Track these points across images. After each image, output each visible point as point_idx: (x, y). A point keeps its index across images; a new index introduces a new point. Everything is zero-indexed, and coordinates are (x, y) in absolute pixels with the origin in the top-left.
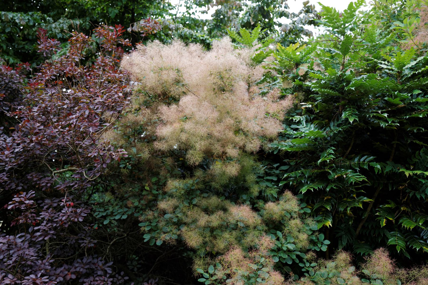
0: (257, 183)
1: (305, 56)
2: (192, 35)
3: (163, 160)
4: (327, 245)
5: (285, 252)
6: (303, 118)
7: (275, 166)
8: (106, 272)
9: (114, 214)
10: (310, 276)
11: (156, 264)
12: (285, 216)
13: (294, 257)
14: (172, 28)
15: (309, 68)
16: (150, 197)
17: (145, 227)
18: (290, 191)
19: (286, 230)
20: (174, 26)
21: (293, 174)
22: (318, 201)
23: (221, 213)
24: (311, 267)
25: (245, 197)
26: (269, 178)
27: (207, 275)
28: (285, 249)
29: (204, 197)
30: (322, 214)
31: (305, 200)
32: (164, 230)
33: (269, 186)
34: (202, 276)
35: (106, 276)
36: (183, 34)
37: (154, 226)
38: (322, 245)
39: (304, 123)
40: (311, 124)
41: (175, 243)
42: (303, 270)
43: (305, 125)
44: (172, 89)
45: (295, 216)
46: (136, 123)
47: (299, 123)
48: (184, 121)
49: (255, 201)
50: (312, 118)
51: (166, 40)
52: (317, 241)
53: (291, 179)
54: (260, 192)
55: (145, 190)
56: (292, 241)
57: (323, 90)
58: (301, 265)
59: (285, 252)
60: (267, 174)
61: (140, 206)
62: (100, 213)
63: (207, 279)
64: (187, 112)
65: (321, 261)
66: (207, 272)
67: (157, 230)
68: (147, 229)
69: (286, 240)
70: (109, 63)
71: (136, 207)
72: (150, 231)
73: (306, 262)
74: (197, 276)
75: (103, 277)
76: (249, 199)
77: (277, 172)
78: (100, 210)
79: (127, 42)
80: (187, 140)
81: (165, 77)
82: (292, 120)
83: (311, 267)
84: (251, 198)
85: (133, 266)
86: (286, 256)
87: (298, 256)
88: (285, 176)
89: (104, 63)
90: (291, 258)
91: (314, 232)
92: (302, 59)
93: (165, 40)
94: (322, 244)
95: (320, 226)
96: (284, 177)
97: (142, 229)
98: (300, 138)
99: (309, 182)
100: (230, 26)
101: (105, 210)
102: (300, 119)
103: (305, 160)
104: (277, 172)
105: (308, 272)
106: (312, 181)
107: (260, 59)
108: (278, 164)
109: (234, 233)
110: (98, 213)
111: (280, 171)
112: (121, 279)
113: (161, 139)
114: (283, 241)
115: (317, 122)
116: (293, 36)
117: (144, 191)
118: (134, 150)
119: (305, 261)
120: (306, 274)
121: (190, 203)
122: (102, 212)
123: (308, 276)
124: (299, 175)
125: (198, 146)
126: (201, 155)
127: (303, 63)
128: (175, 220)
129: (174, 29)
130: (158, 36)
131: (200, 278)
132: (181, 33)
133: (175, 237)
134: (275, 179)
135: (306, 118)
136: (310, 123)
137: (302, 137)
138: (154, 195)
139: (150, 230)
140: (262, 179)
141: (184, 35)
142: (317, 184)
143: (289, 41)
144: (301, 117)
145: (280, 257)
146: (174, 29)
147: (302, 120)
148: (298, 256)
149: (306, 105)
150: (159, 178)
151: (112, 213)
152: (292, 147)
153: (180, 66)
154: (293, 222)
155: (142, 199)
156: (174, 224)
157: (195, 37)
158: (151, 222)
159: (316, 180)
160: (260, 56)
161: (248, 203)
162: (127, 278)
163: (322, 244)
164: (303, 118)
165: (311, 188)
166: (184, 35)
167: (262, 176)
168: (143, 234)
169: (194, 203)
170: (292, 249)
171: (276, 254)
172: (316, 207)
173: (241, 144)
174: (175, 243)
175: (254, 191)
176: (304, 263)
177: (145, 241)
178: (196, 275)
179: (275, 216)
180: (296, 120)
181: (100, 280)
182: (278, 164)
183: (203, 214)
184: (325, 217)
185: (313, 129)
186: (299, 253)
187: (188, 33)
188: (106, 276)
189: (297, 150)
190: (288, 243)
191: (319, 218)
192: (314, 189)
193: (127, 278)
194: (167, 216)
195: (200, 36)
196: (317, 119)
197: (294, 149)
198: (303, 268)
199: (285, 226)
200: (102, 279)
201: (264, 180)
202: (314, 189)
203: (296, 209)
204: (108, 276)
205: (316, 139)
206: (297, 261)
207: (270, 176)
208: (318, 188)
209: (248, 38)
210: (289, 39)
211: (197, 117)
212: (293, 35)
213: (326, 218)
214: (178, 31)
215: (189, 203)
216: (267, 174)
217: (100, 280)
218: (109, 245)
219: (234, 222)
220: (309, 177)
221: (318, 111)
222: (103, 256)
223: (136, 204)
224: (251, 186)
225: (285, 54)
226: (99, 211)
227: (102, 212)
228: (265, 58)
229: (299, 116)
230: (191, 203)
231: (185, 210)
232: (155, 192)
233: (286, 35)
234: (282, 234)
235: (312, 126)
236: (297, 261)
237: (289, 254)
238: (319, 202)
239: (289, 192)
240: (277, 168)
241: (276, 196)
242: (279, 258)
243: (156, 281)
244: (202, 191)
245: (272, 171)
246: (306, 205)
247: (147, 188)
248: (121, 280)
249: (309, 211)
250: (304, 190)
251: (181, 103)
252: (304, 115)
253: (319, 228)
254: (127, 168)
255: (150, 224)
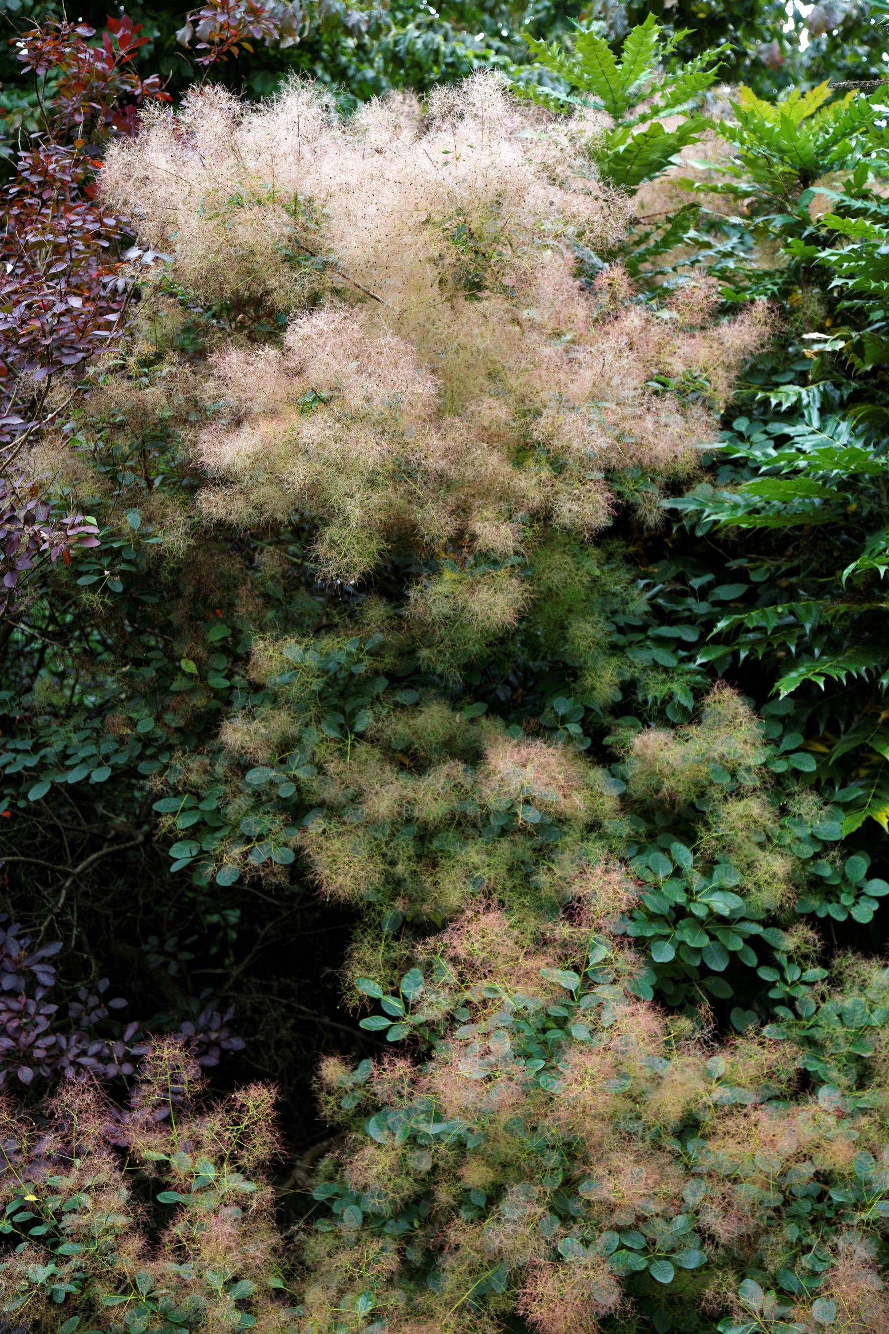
0: (615, 649)
1: (835, 142)
2: (437, 52)
3: (286, 551)
4: (879, 899)
5: (700, 923)
6: (811, 396)
7: (696, 583)
8: (33, 983)
9: (67, 763)
10: (798, 1017)
11: (257, 947)
12: (711, 783)
13: (737, 944)
14: (356, 26)
15: (847, 193)
16: (200, 701)
17: (174, 814)
18: (732, 685)
19: (707, 839)
20: (364, 16)
21: (753, 618)
22: (854, 725)
23: (456, 769)
24: (805, 983)
25: (562, 705)
26: (666, 631)
27: (394, 1005)
28: (699, 911)
29: (396, 704)
30: (868, 777)
31: (804, 719)
32: (243, 829)
33: (662, 662)
34: (375, 1007)
35: (31, 996)
36: (401, 47)
37: (212, 812)
38: (857, 897)
39: (815, 415)
40: (843, 419)
41: (282, 879)
42: (773, 994)
43: (816, 424)
44: (272, 283)
45: (749, 781)
46: (139, 414)
47: (795, 413)
48: (304, 410)
49: (608, 720)
50: (846, 394)
51: (358, 70)
52: (836, 882)
53: (751, 636)
54: (629, 687)
55: (184, 674)
56: (732, 882)
57: (873, 285)
58: (766, 974)
59: (700, 923)
60: (660, 615)
61: (159, 732)
62: (19, 757)
63: (394, 1019)
64: (316, 375)
65: (845, 961)
66: (395, 994)
67: (219, 828)
68: (183, 823)
69: (707, 872)
70: (58, 175)
71: (146, 741)
72: (194, 833)
73: (784, 962)
74: (355, 1009)
75: (23, 999)
76: (581, 716)
77: (702, 608)
78: (20, 745)
79: (152, 85)
80: (314, 489)
81: (245, 234)
82: (766, 401)
83: (805, 983)
84: (588, 710)
85: (166, 954)
86: (705, 941)
87: (754, 942)
88: (721, 625)
89: (40, 174)
90: (724, 947)
91: (827, 846)
92: (825, 150)
93: (351, 72)
94: (859, 893)
95: (853, 823)
96: (715, 631)
97: (166, 822)
98: (788, 476)
99: (817, 652)
100: (590, 13)
101: (36, 748)
102: (800, 400)
103: (808, 562)
104: (702, 608)
105: (790, 1002)
106: (833, 648)
107: (655, 156)
108: (709, 577)
109: (504, 845)
110: (13, 755)
111: (714, 604)
112: (95, 1008)
113: (224, 480)
114: (697, 880)
115: (862, 409)
116: (863, 50)
117: (179, 677)
118: (132, 520)
119: (782, 959)
120: (781, 1011)
121: (345, 729)
122: (26, 752)
123: (791, 1016)
124: (774, 623)
125: (354, 511)
126: (373, 546)
127: (829, 169)
128: (287, 791)
129: (364, 28)
130: (324, 54)
131: (364, 1015)
132: (396, 43)
133: (283, 856)
134: (690, 635)
135: (824, 395)
136: (840, 414)
137: (796, 472)
138: (216, 694)
139: (198, 824)
140: (642, 637)
141: (408, 52)
142: (850, 659)
143: (845, 67)
144: (803, 391)
145: (681, 945)
146: (364, 28)
147: (805, 402)
148: (754, 942)
149: (826, 341)
150: (233, 628)
151: (64, 755)
152: (757, 511)
153: (308, 188)
154: (735, 809)
155: (166, 709)
156: (283, 805)
157: (450, 60)
158: (200, 799)
159: (846, 643)
160: (652, 141)
161: (575, 729)
162: (118, 1003)
163: (859, 893)
164: (811, 396)
165: (820, 674)
166: (408, 52)
167: (638, 623)
168: (169, 840)
169: (359, 728)
170: (726, 913)
171: (667, 931)
172: (843, 746)
173: (536, 498)
174: (282, 879)
175: (598, 685)
176: (780, 969)
177: (174, 868)
178: (354, 1003)
179: (668, 784)
180: (779, 404)
181: (9, 1010)
182: (709, 577)
183: (389, 772)
184: (878, 787)
185: (845, 439)
186: (756, 929)
187: (419, 44)
188: (31, 996)
189: (773, 524)
190: (714, 890)
191: (854, 792)
192: (829, 680)
193: (118, 1003)
194: (255, 777)
195: (471, 56)
196: (872, 400)
197: (758, 522)
198: (773, 985)
199: (706, 824)
200: (15, 1005)
201: (648, 637)
202: (829, 680)
203: (755, 757)
204: (40, 994)
205: (851, 483)
206: (751, 960)
207: (672, 623)
208: (849, 676)
209: (608, 72)
210: (849, 62)
211: (355, 401)
212: (863, 43)
213: (880, 793)
214: (382, 38)
215: (341, 726)
216: (660, 615)
217: (9, 1010)
218: (66, 875)
219: (504, 805)
220: (819, 630)
221: (869, 368)
222: (45, 917)
223: (146, 725)
224: (590, 663)
225: (754, 131)
226: (16, 751)
227: (26, 752)
228: (676, 150)
229: (797, 388)
230: (352, 727)
231: (322, 752)
232: (219, 682)
233: (834, 45)
234: (695, 852)
235: (844, 426)
236: (751, 960)
237: (718, 934)
238: (856, 730)
239: (728, 692)
240: (703, 594)
241: (687, 702)
242: (677, 950)
243: (226, 1019)
244: (396, 680)
245: (678, 603)
246: (801, 741)
247: (189, 666)
248: (99, 1012)
249: (809, 765)
250: (786, 686)
251: (291, 338)
252: (814, 382)
253: (845, 833)
254: (106, 589)
255: (193, 802)
